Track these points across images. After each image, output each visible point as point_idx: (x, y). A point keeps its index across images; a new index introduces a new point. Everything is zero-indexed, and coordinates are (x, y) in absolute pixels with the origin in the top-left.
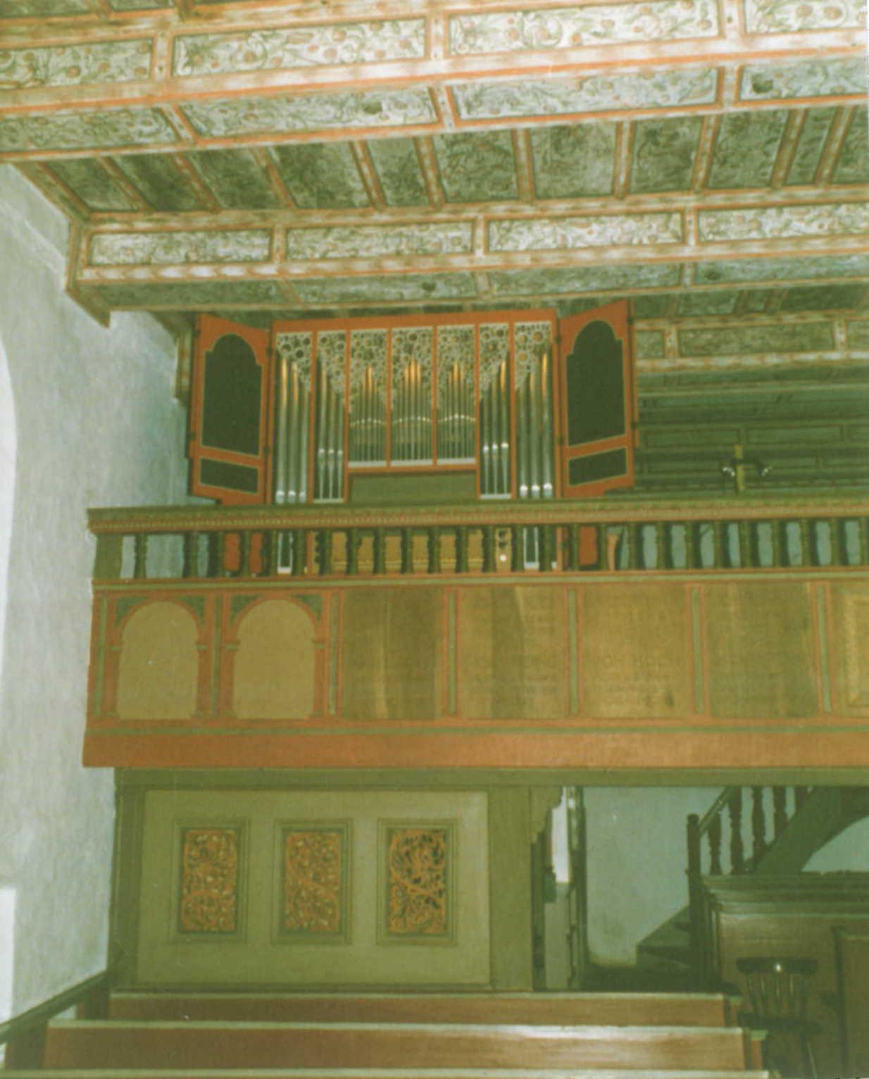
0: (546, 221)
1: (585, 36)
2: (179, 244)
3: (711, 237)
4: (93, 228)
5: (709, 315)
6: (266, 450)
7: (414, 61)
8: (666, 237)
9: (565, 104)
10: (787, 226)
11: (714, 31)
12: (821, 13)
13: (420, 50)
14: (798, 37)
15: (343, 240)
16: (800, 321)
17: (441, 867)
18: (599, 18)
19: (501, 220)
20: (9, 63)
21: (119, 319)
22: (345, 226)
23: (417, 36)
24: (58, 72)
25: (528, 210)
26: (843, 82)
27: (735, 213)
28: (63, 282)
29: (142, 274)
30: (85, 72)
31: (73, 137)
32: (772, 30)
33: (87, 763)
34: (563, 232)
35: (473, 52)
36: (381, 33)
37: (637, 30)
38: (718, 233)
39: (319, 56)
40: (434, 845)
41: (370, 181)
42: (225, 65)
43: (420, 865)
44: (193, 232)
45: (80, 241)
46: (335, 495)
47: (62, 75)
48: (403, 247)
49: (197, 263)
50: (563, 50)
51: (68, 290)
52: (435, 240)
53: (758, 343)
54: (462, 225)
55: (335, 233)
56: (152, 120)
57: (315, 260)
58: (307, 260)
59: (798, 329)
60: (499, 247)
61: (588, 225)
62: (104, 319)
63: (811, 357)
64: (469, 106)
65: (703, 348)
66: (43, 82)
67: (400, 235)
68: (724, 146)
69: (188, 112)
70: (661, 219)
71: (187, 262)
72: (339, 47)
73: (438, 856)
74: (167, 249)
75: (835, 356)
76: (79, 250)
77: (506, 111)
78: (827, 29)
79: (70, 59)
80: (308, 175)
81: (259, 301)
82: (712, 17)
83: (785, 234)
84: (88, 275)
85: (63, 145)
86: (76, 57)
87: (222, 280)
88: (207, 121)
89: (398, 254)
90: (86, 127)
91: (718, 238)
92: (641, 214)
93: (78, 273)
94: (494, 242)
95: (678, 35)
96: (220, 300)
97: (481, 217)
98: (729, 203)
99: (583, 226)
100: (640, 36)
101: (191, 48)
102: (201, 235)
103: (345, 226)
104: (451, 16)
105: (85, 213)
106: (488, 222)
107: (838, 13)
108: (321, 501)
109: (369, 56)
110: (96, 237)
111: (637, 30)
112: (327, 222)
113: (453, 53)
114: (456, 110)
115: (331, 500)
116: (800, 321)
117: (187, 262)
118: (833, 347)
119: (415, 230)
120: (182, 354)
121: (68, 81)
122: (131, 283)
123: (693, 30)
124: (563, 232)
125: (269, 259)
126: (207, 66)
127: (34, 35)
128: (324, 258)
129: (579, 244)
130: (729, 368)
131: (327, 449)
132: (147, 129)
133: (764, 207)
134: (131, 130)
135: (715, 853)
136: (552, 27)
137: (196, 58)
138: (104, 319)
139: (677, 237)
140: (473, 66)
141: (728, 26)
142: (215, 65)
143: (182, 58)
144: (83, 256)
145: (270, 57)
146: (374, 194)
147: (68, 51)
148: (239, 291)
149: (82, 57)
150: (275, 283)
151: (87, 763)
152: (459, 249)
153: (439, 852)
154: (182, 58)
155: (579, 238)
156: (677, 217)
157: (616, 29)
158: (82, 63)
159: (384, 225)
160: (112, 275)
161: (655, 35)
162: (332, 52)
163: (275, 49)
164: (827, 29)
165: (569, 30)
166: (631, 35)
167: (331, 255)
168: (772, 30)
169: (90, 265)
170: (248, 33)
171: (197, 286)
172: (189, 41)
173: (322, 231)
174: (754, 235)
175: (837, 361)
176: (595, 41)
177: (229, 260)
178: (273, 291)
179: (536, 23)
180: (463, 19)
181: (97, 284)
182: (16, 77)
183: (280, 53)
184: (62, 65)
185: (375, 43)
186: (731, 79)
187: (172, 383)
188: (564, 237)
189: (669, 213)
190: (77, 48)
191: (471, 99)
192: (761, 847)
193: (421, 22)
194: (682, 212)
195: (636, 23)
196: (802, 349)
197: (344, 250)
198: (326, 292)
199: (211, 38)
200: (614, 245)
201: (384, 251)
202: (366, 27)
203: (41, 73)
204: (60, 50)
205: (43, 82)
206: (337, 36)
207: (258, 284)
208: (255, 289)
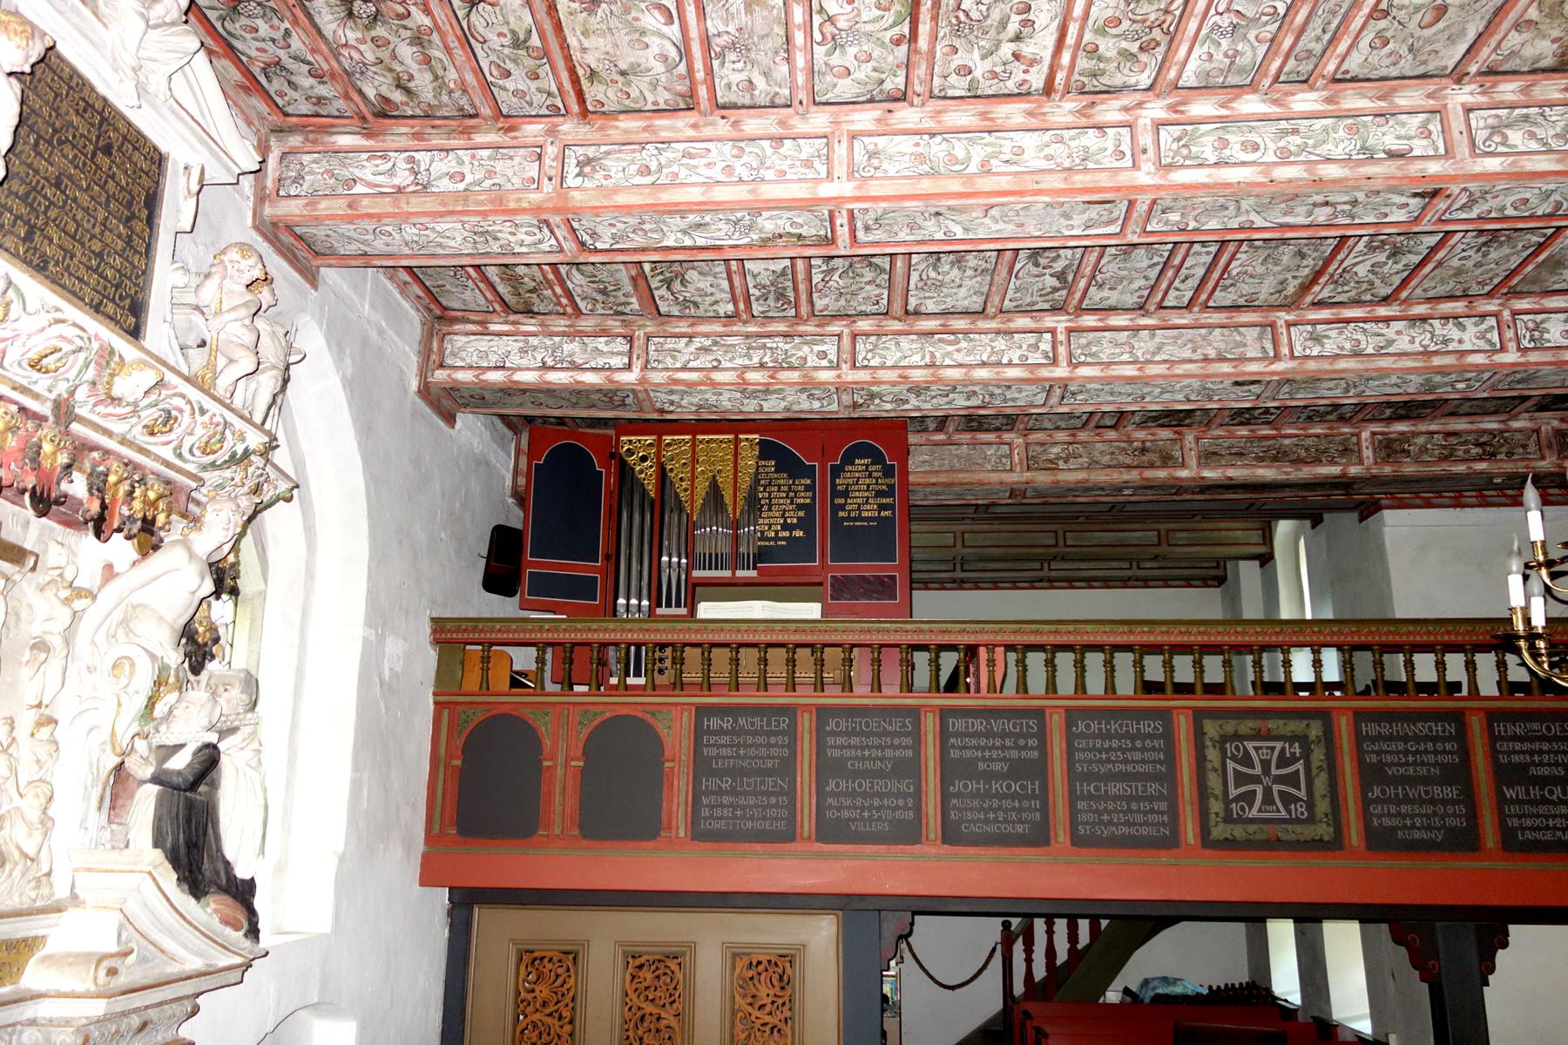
0: (915, 337)
1: (994, 162)
2: (535, 348)
3: (1082, 358)
4: (445, 329)
5: (1058, 428)
6: (607, 557)
7: (817, 181)
8: (1035, 358)
9: (966, 230)
10: (1159, 349)
11: (1128, 162)
12: (1238, 146)
13: (823, 171)
14: (1213, 171)
15: (706, 350)
16: (1150, 437)
17: (788, 992)
18: (1008, 144)
19: (867, 335)
20: (390, 164)
21: (463, 419)
22: (707, 335)
23: (819, 156)
24: (439, 178)
25: (897, 326)
26: (1253, 217)
27: (1106, 334)
28: (414, 384)
29: (495, 377)
30: (469, 178)
31: (452, 243)
32: (1188, 162)
33: (422, 884)
34: (931, 349)
35: (878, 175)
36: (781, 151)
37: (1049, 158)
38: (1090, 355)
39: (716, 173)
40: (780, 971)
41: (738, 291)
42: (617, 176)
43: (764, 992)
44: (551, 335)
45: (431, 343)
46: (678, 605)
47: (446, 181)
48: (766, 359)
49: (553, 368)
50: (972, 176)
51: (419, 391)
52: (800, 354)
53: (1106, 459)
54: (827, 339)
55: (698, 342)
56: (537, 231)
57: (677, 370)
58: (667, 369)
59: (1148, 444)
60: (866, 363)
61: (957, 342)
62: (450, 419)
63: (1161, 474)
64: (867, 228)
65: (1051, 461)
66: (425, 187)
67: (764, 346)
68: (1104, 270)
69: (575, 225)
70: (1031, 338)
71: (545, 367)
72: (737, 164)
73: (784, 981)
74: (523, 351)
75: (1184, 473)
76: (430, 350)
77: (903, 235)
78: (1244, 163)
79: (454, 163)
80: (677, 286)
81: (615, 408)
82: (1126, 148)
83: (1158, 358)
84: (440, 375)
85: (440, 251)
86: (461, 162)
87: (579, 387)
88: (594, 235)
89: (762, 366)
90: (466, 234)
91: (1089, 360)
92: (1010, 333)
93: (429, 374)
94: (860, 358)
95: (1090, 165)
96: (574, 406)
97: (846, 331)
98: (1100, 324)
99: (950, 343)
100: (1050, 165)
101: (581, 158)
102: (557, 339)
103: (707, 335)
104: (853, 136)
105: (438, 312)
106: (854, 336)
107: (1256, 147)
108: (659, 611)
109: (769, 175)
110: (448, 337)
111: (1049, 158)
112: (689, 330)
113: (856, 175)
114: (853, 232)
115: (673, 611)
116: (1150, 437)
117: (545, 367)
118: (1183, 465)
119: (780, 343)
120: (518, 452)
121: (452, 187)
122: (485, 386)
123: (1109, 162)
124: (931, 349)
125: (629, 367)
126: (600, 175)
127: (417, 136)
128: (684, 369)
129: (948, 362)
130: (1078, 482)
131: (670, 557)
132: (528, 240)
133: (1136, 330)
134: (512, 239)
135: (1029, 961)
136: (960, 152)
137: (587, 169)
138: (450, 419)
139: (1047, 357)
140: (875, 189)
141: (1144, 157)
142: (607, 177)
143: (572, 169)
144: (434, 357)
145: (665, 171)
146: (742, 306)
147: (452, 155)
148: (595, 397)
149: (467, 162)
150: (633, 391)
151: (422, 884)
152: (824, 363)
153: (785, 978)
154: (572, 169)
155: (949, 354)
156: (1048, 336)
157: (1025, 156)
158: (466, 170)
159: (747, 336)
160: (464, 376)
161: (1067, 164)
162: (728, 169)
163: (670, 163)
164: (1244, 163)
165: (978, 154)
166: (1045, 165)
167: (691, 365)
168: (1188, 162)
169: (441, 366)
170: (643, 145)
171: (551, 392)
172: (580, 150)
173: (685, 340)
174: (1126, 357)
175: (1187, 479)
176: (1006, 168)
177: (587, 366)
178: (629, 400)
179: (944, 145)
180: (866, 140)
181: (448, 386)
182: (397, 181)
183: (675, 168)
184: (445, 170)
185: (774, 160)
186: (1142, 208)
187: (509, 483)
188: (933, 355)
189: (1039, 332)
190: (460, 153)
191: (870, 222)
192: (1073, 951)
193: (825, 140)
194: (1053, 332)
195: (1047, 151)
196: (1152, 466)
197: (705, 361)
198: (684, 403)
199: (603, 148)
200: (984, 364)
201: (747, 362)
202: (766, 144)
203: (422, 178)
204: (443, 154)
205: (425, 187)
206: (735, 152)
207: (615, 392)
208: (611, 395)
